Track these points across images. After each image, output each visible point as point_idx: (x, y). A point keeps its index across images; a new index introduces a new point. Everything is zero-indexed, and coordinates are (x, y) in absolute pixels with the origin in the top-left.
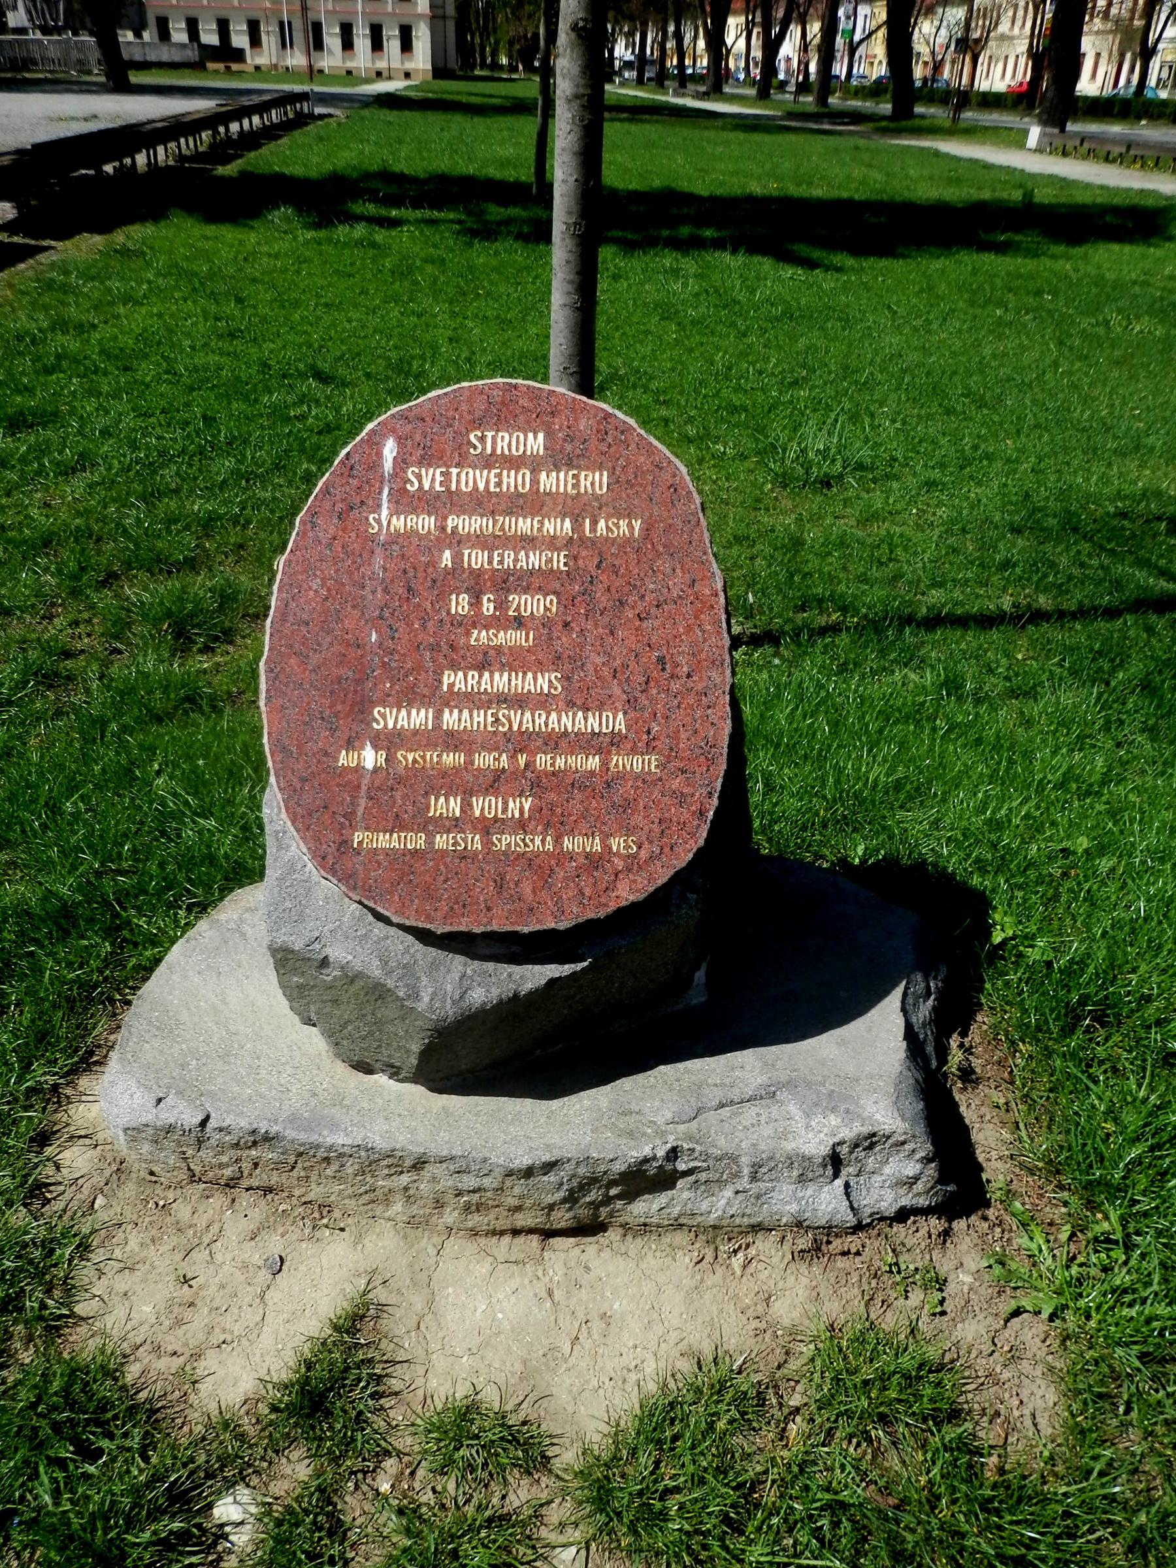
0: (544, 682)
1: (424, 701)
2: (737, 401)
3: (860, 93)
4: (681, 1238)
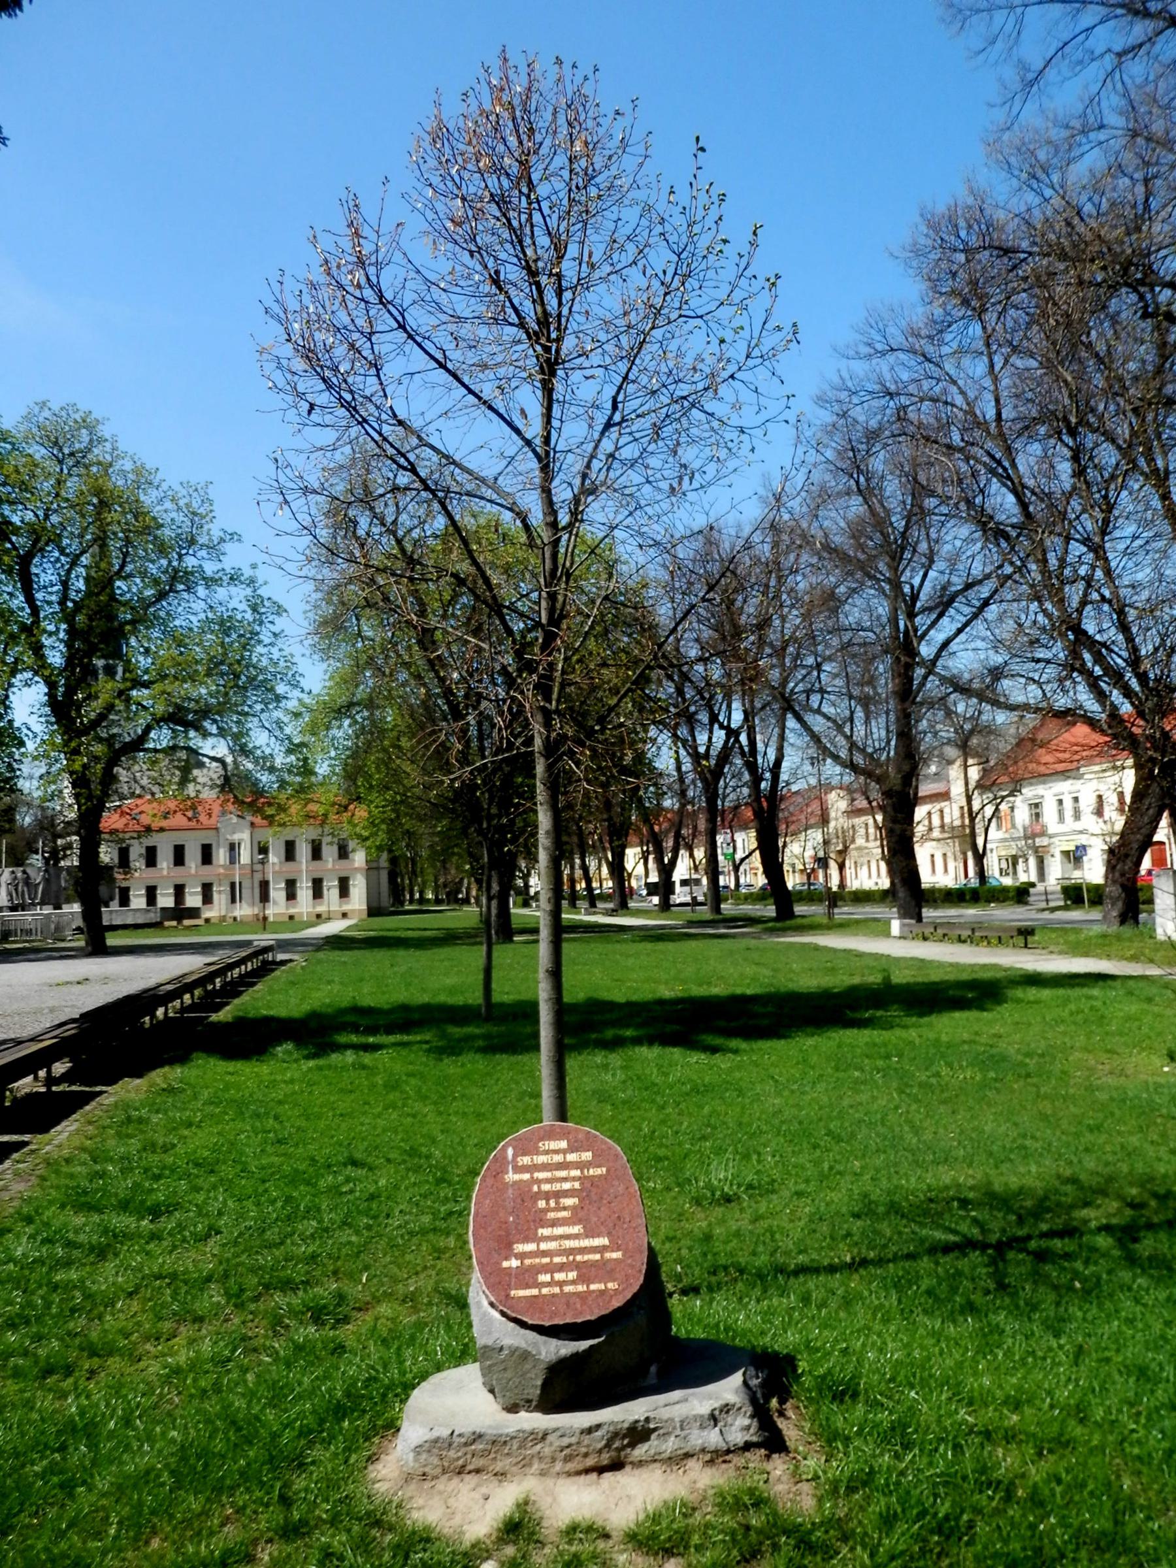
0: (576, 1229)
1: (533, 1241)
2: (662, 1152)
3: (750, 898)
4: (657, 1465)
